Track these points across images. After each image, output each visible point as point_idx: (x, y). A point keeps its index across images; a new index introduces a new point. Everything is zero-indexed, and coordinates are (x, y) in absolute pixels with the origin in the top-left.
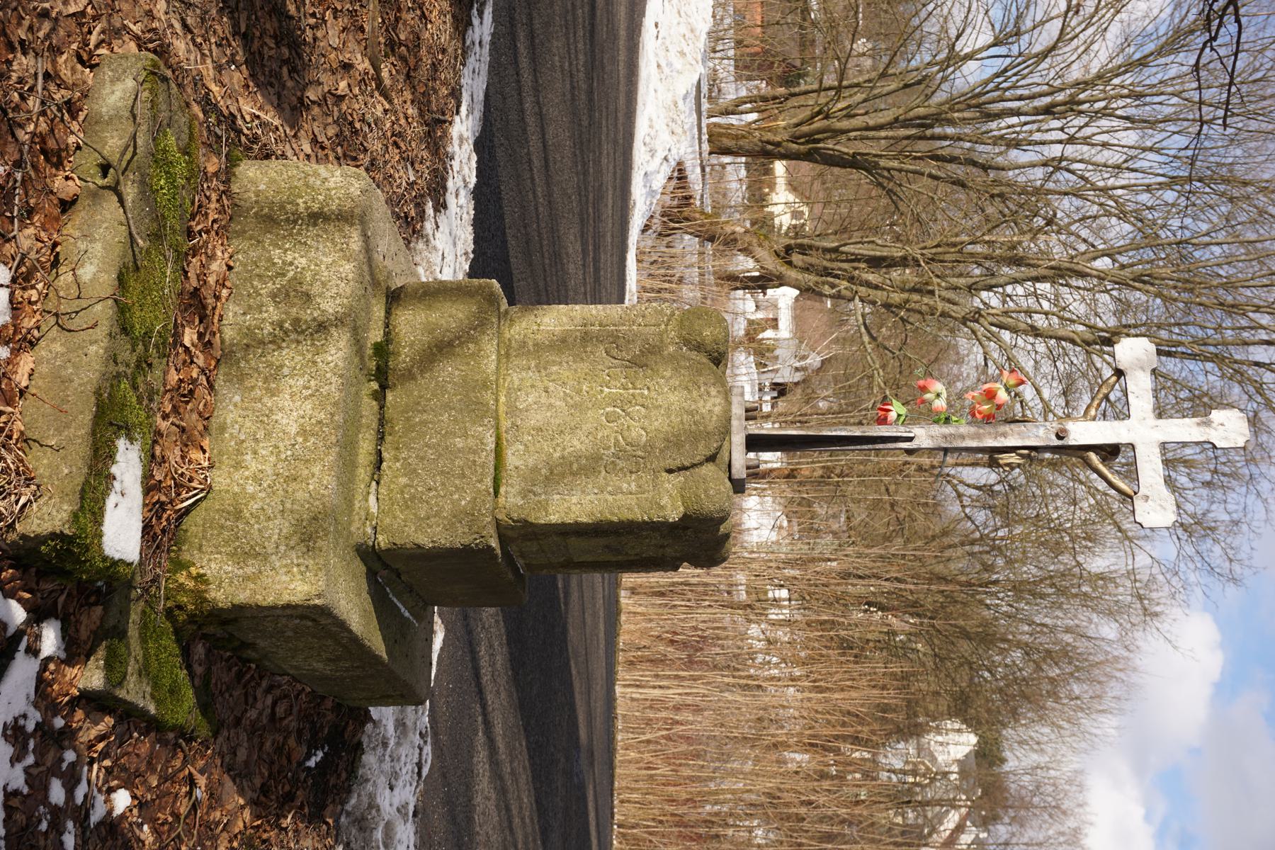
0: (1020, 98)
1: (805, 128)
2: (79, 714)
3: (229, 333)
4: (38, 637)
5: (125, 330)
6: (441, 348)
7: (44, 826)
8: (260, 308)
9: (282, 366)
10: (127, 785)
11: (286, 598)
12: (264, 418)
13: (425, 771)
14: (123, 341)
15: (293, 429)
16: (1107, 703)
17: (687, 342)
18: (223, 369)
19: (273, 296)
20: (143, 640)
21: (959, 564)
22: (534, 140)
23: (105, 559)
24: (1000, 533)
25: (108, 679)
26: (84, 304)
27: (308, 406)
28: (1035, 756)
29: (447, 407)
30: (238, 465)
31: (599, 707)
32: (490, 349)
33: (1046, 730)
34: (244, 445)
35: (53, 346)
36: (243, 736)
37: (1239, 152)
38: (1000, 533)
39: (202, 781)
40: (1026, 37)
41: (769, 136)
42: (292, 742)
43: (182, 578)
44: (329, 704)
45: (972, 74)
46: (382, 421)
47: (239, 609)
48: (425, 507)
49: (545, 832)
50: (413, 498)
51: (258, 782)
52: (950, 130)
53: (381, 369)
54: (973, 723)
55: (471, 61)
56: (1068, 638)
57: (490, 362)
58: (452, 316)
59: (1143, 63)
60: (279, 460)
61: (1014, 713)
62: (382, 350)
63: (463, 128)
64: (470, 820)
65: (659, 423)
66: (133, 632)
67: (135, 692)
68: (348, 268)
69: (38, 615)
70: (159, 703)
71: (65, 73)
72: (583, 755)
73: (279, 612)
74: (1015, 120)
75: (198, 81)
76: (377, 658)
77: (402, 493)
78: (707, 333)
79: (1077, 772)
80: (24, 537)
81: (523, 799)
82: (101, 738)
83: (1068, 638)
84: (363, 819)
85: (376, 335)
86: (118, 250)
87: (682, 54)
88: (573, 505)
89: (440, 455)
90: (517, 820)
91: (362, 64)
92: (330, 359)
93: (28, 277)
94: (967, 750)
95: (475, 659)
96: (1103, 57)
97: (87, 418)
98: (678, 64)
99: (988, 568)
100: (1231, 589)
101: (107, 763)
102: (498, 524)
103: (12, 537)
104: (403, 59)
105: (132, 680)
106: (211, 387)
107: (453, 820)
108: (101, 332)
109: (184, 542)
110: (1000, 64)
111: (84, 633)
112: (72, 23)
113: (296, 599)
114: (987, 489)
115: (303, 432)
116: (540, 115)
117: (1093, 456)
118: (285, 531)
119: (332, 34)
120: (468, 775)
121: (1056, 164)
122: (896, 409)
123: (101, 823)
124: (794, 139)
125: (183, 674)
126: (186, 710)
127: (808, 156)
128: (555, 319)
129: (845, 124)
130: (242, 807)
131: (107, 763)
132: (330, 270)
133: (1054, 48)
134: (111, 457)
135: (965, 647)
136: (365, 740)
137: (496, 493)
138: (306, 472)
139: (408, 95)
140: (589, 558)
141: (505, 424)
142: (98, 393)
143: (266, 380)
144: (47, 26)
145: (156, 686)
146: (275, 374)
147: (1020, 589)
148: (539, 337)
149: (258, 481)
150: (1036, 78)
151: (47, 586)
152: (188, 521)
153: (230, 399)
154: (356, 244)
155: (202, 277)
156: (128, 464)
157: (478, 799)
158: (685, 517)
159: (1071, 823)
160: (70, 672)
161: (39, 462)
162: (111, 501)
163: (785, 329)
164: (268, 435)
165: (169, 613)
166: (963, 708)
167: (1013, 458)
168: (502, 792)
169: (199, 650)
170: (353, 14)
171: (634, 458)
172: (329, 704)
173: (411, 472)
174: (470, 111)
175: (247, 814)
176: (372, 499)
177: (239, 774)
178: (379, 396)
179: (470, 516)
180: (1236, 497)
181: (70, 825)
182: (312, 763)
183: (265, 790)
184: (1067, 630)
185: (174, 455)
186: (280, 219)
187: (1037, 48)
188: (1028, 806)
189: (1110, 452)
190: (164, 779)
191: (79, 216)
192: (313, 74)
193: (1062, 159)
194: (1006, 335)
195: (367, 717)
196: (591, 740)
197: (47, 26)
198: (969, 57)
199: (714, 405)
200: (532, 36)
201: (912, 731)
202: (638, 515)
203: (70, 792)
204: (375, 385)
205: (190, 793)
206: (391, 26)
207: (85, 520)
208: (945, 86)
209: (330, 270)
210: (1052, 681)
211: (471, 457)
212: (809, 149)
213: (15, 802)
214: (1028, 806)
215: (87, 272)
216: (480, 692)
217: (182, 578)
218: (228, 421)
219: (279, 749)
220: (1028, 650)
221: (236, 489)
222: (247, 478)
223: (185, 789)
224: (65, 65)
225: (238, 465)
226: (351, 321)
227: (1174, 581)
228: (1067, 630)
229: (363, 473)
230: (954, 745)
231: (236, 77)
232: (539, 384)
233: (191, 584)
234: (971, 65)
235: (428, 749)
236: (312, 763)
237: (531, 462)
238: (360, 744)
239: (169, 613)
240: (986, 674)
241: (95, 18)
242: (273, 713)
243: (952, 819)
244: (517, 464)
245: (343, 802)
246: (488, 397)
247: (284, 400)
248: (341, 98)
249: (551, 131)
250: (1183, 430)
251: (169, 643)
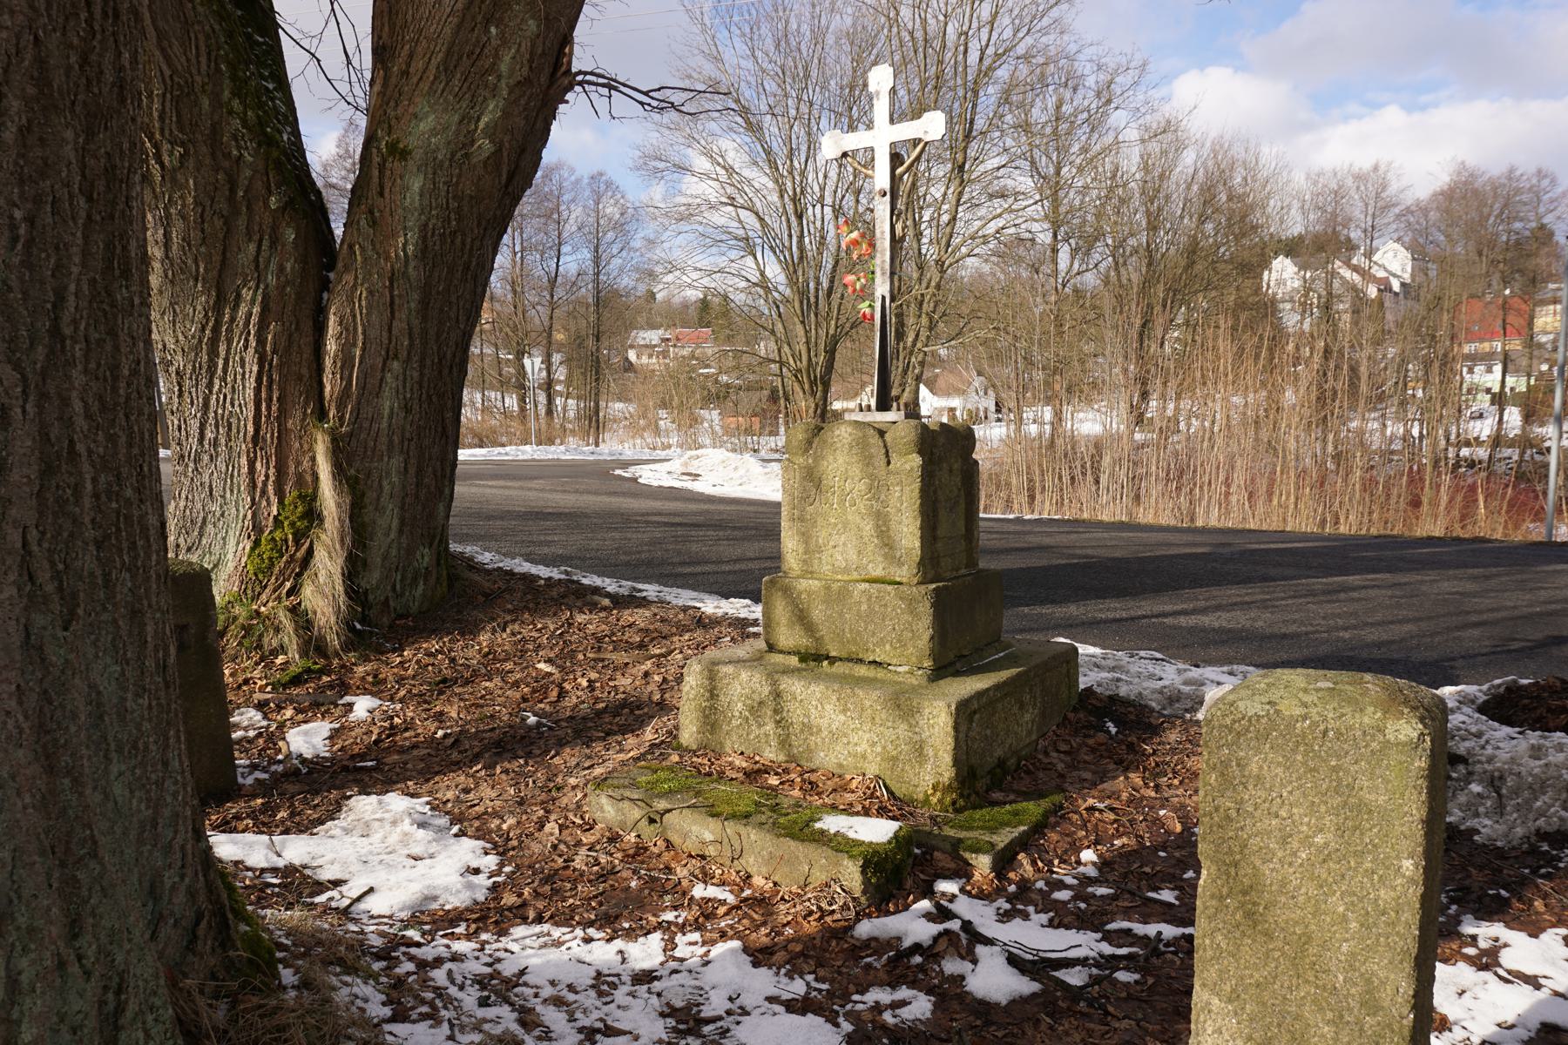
0: (790, 236)
1: (807, 387)
2: (1012, 875)
3: (782, 758)
4: (943, 894)
5: (747, 816)
6: (802, 618)
7: (1083, 906)
8: (767, 735)
10: (1078, 851)
11: (950, 729)
12: (835, 736)
13: (1158, 655)
14: (754, 819)
15: (842, 718)
16: (1251, 158)
17: (807, 451)
18: (803, 763)
19: (760, 726)
20: (971, 828)
21: (1134, 272)
22: (751, 565)
23: (889, 842)
24: (1110, 241)
25: (986, 852)
26: (726, 841)
28: (1293, 211)
29: (841, 614)
30: (864, 757)
31: (1189, 538)
32: (803, 584)
33: (1272, 202)
35: (750, 863)
36: (1075, 773)
37: (832, 83)
38: (1110, 241)
39: (1091, 801)
40: (751, 234)
41: (811, 411)
42: (1091, 742)
43: (934, 800)
44: (1071, 715)
45: (775, 272)
46: (849, 660)
47: (956, 762)
48: (903, 633)
49: (1265, 579)
50: (899, 641)
51: (1112, 766)
52: (812, 285)
53: (813, 658)
54: (1265, 263)
55: (668, 598)
56: (1195, 188)
57: (815, 584)
58: (781, 610)
59: (768, 152)
61: (1254, 228)
62: (804, 658)
63: (711, 606)
64: (1230, 630)
65: (856, 470)
66: (962, 834)
67: (1003, 839)
68: (744, 675)
69: (928, 892)
70: (1021, 823)
71: (592, 839)
72: (1221, 550)
73: (962, 735)
74: (807, 240)
75: (623, 763)
76: (1018, 674)
78: (800, 437)
79: (1308, 177)
80: (864, 892)
81: (1233, 593)
82: (1034, 863)
83: (1195, 188)
84: (1170, 698)
85: (794, 661)
86: (696, 816)
87: (736, 469)
88: (909, 534)
90: (1247, 599)
91: (648, 665)
93: (705, 874)
94: (1288, 261)
95: (1106, 621)
96: (765, 180)
97: (792, 843)
98: (742, 472)
99: (1135, 251)
100: (1151, 67)
101: (1056, 862)
102: (919, 583)
103: (863, 900)
104: (653, 640)
105: (995, 838)
106: (813, 771)
107: (1223, 642)
108: (743, 830)
110: (767, 251)
111: (952, 865)
112: (565, 832)
113: (950, 723)
114: (1074, 252)
115: (844, 711)
116: (736, 561)
117: (899, 171)
119: (624, 682)
120: (1192, 630)
121: (837, 211)
122: (864, 307)
123: (1100, 870)
124: (813, 394)
125: (1008, 807)
126: (1034, 809)
127: (826, 386)
128: (790, 543)
129: (805, 358)
130: (1127, 778)
131: (1056, 862)
132: (743, 685)
133: (757, 214)
134: (822, 832)
135: (1199, 267)
136: (1108, 693)
137: (900, 583)
139: (676, 639)
140: (961, 524)
141: (855, 576)
142: (779, 836)
144: (562, 847)
145: (1008, 824)
146: (807, 727)
147: (1153, 227)
149: (874, 744)
150: (776, 226)
151: (909, 883)
152: (898, 794)
154: (729, 669)
155: (739, 769)
156: (832, 823)
157: (1216, 625)
158: (920, 452)
159: (1349, 182)
160: (977, 877)
161: (819, 877)
162: (851, 835)
163: (956, 402)
164: (845, 735)
165: (957, 811)
166: (1254, 266)
167: (899, 227)
168: (1218, 608)
169: (997, 796)
170: (615, 669)
171: (876, 488)
172: (1071, 715)
173: (882, 642)
174: (702, 601)
175: (1132, 775)
176: (900, 669)
177: (1103, 777)
178: (832, 660)
179: (911, 602)
180: (1084, 67)
181: (1090, 889)
182: (1113, 730)
183: (1119, 762)
184: (1189, 187)
185: (849, 797)
186: (711, 718)
187: (758, 225)
188: (1334, 215)
189: (896, 159)
190: (1084, 826)
191: (676, 839)
192: (645, 697)
193: (833, 206)
194: (956, 241)
195: (1089, 690)
196: (1205, 545)
197: (562, 847)
198: (762, 274)
200: (683, 564)
201: (1267, 308)
202: (917, 485)
203: (1067, 887)
204: (825, 663)
205: (1101, 811)
206: (630, 646)
207: (855, 851)
208: (781, 288)
209: (743, 685)
210: (1230, 199)
212: (821, 384)
213: (1056, 922)
214: (1334, 215)
215: (708, 837)
216: (1132, 619)
219: (1093, 750)
220: (1203, 219)
223: (1097, 814)
224: (587, 839)
225: (864, 757)
226: (773, 675)
227: (1143, 110)
228: (1189, 187)
229: (880, 674)
230: (1283, 274)
231: (631, 741)
234: (769, 273)
235: (1142, 653)
236: (1113, 730)
237: (880, 559)
238: (1110, 697)
239: (957, 811)
240: (1222, 250)
241: (566, 818)
242: (1064, 752)
243: (1347, 274)
245: (1152, 710)
246: (835, 586)
247: (824, 723)
248: (665, 679)
249: (750, 554)
250: (881, 109)
251: (978, 814)
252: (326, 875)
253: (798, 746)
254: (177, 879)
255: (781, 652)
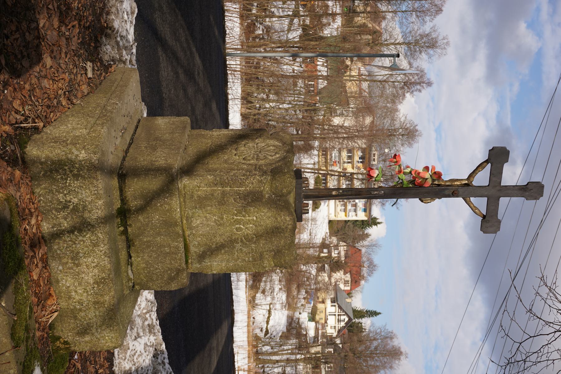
9: (78, 253)
15: (92, 281)
27: (96, 271)
34: (70, 289)
60: (88, 295)
77: (144, 270)
89: (159, 255)
92: (102, 249)
109: (54, 329)
115: (96, 282)
118: (98, 324)
138: (102, 300)
143: (72, 259)
148: (199, 193)
153: (57, 268)
164: (80, 284)
199: (288, 225)
211: (174, 256)
217: (58, 344)
218: (59, 278)
221: (72, 307)
222: (75, 302)
225: (70, 298)
232: (201, 215)
233: (62, 346)
244: (195, 250)
247: (84, 268)
252: (384, 325)
253: (58, 246)
254: (238, 246)
255: (121, 190)
